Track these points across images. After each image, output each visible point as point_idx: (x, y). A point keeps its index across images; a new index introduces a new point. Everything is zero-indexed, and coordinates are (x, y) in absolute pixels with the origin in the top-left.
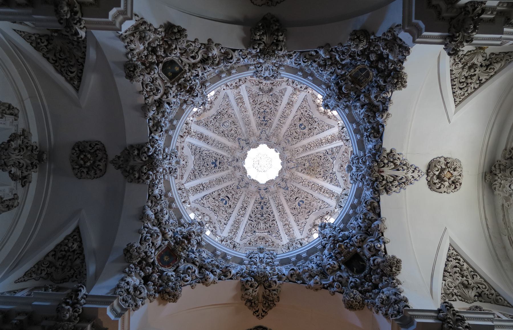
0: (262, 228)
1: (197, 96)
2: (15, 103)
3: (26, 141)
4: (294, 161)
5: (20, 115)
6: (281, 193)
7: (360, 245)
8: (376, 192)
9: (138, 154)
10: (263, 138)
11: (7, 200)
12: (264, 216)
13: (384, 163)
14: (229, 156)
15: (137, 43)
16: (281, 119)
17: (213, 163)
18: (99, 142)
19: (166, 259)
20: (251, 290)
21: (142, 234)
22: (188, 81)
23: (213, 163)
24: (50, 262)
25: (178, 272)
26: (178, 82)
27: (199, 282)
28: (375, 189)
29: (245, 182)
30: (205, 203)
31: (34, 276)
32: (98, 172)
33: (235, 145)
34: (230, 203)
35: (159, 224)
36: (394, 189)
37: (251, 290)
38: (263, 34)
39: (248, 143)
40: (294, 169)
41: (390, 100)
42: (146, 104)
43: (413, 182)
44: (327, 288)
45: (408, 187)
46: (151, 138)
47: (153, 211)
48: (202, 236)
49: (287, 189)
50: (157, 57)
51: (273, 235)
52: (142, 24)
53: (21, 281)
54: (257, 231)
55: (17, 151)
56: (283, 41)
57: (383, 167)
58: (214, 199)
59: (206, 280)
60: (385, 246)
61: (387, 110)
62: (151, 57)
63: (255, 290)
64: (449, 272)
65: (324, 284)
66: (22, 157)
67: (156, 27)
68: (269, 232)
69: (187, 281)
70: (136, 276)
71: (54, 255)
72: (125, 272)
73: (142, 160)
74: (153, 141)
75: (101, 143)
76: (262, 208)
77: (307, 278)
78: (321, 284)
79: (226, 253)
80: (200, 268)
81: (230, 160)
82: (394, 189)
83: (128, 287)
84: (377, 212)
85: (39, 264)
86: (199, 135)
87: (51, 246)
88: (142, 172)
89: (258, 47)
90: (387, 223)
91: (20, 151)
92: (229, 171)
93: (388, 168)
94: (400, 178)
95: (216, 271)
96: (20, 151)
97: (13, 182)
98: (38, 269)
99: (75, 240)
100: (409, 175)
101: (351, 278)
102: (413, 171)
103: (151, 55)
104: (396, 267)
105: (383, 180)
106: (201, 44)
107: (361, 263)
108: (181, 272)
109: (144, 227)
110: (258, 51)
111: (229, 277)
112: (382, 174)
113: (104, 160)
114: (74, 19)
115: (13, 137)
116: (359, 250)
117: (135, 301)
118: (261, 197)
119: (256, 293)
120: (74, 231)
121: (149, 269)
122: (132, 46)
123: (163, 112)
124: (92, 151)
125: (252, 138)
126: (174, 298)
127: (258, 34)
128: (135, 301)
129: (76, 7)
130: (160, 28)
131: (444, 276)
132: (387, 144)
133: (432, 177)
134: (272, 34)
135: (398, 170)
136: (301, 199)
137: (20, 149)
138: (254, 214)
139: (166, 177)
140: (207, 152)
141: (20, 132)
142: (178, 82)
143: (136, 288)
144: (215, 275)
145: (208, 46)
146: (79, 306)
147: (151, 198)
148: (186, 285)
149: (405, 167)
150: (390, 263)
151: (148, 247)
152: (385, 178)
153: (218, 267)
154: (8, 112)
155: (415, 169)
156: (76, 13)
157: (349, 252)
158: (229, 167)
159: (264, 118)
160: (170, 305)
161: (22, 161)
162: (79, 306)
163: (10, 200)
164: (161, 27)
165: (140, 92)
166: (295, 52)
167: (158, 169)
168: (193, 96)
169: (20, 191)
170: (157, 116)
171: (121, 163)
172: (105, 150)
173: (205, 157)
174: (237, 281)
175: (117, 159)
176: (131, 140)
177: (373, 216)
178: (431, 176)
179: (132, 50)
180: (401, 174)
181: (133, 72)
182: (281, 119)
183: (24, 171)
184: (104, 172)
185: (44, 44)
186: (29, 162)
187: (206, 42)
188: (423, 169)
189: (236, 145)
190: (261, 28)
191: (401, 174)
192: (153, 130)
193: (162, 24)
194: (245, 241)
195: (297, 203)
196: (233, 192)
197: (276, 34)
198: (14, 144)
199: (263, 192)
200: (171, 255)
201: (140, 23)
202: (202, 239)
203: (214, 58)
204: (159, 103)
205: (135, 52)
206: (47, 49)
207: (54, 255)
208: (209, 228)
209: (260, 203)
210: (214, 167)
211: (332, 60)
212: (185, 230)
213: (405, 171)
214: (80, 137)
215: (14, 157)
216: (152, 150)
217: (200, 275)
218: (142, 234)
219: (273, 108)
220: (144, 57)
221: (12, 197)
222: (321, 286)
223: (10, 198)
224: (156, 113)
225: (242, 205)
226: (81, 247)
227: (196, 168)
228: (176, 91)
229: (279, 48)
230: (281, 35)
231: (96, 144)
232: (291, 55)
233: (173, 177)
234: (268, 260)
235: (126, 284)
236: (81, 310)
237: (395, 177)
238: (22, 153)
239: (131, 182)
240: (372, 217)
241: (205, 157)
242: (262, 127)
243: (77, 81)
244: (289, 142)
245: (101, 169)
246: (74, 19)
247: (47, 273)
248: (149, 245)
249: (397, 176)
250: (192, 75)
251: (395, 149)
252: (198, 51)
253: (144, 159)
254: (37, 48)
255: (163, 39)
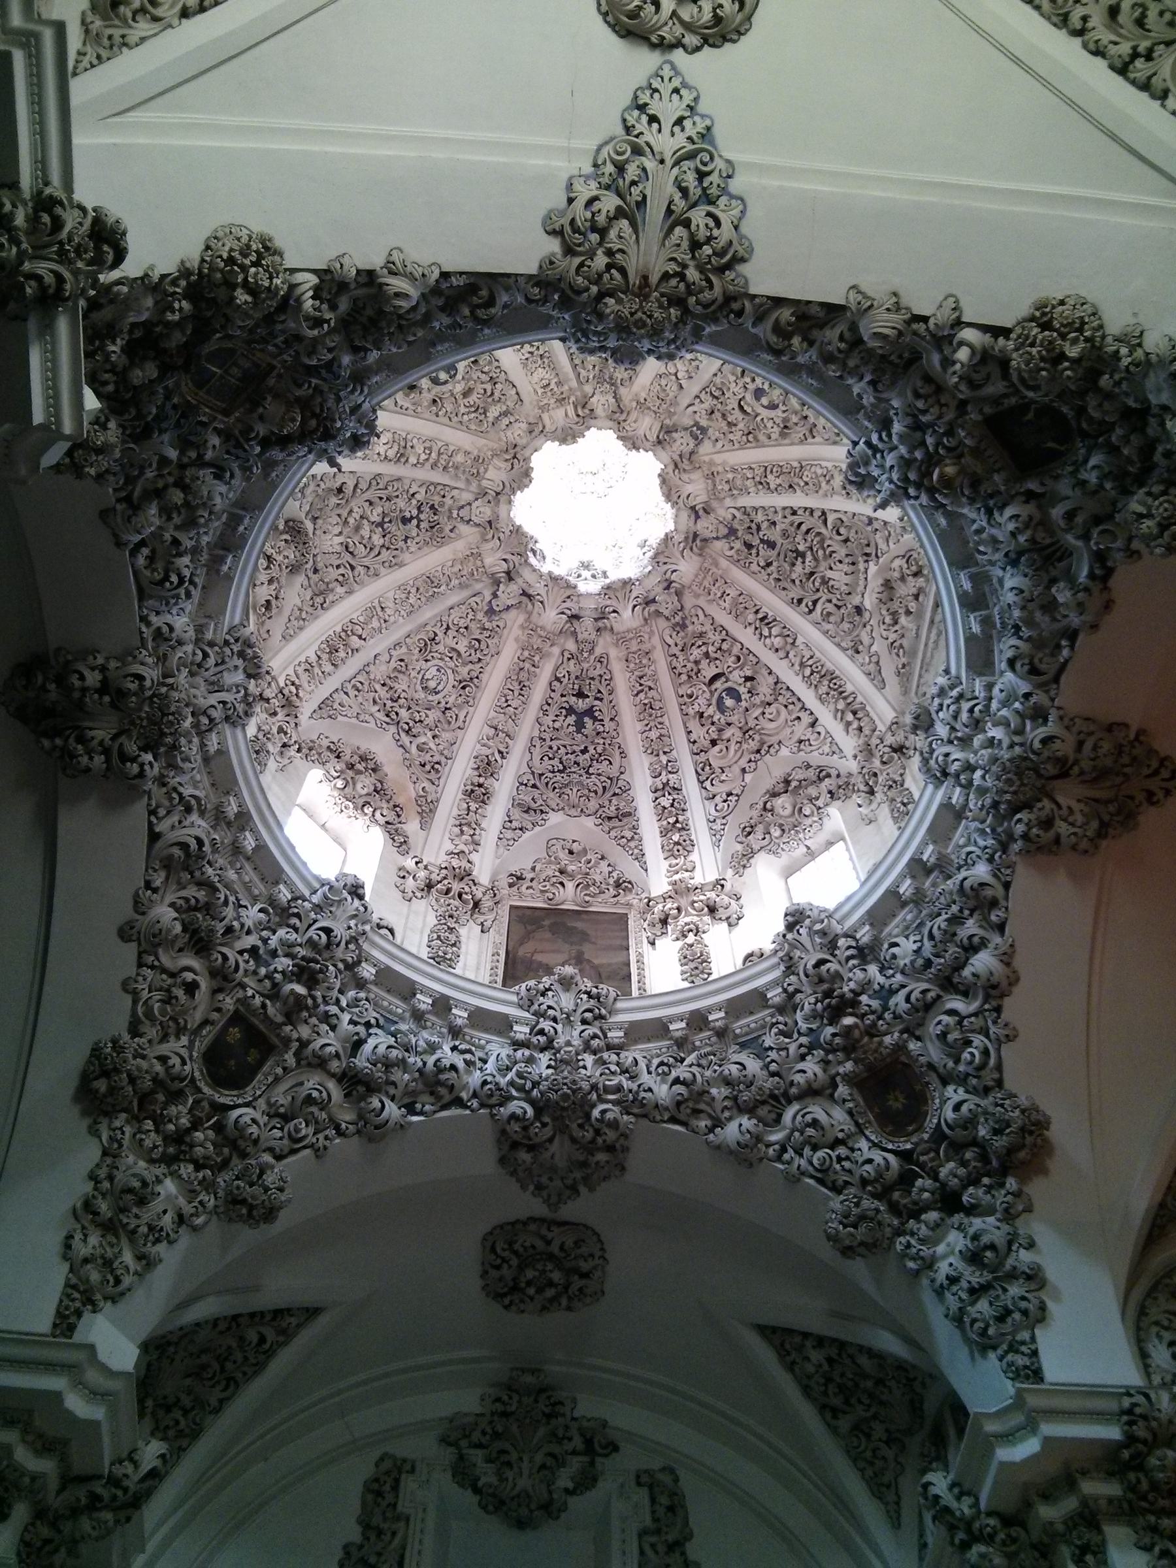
0: (847, 579)
1: (328, 931)
2: (362, 1468)
3: (476, 1436)
4: (588, 389)
5: (403, 1449)
6: (718, 458)
7: (953, 404)
8: (732, 304)
9: (531, 1148)
10: (487, 512)
11: (653, 1512)
12: (801, 548)
13: (609, 267)
14: (556, 650)
15: (156, 1206)
16: (413, 460)
17: (580, 726)
18: (484, 1239)
19: (897, 1102)
20: (1062, 827)
21: (803, 1174)
22: (275, 985)
23: (580, 726)
24: (856, 1428)
25: (950, 1074)
26: (280, 1026)
27: (998, 1010)
28: (721, 307)
29: (661, 598)
30: (725, 788)
31: (888, 1477)
32: (584, 1250)
33: (516, 631)
34: (736, 677)
35: (777, 1100)
36: (725, 233)
37: (1062, 827)
38: (81, 740)
39: (508, 573)
40: (623, 391)
41: (327, 271)
42: (358, 1132)
43: (701, 126)
44: (1109, 572)
45: (728, 147)
46: (475, 1103)
47: (727, 1114)
48: (839, 929)
49: (704, 430)
50: (196, 1125)
51: (882, 546)
52: (96, 1214)
53: (898, 1512)
54: (856, 600)
55: (509, 1474)
56: (103, 669)
57: (623, 271)
58: (714, 743)
59: (994, 987)
60: (970, 325)
61: (371, 273)
62: (199, 1151)
63: (1065, 812)
64: (1135, 55)
65: (1092, 576)
66: (526, 1458)
67: (98, 1153)
68: (867, 555)
69: (986, 1052)
70: (936, 1243)
71: (835, 1412)
72: (917, 1273)
73: (551, 1140)
74: (492, 1097)
75: (491, 1233)
76: (771, 545)
77: (1054, 619)
78: (1087, 590)
79: (912, 860)
80: (949, 983)
81: (571, 646)
82: (725, 233)
83: (964, 1284)
84: (822, 314)
85: (855, 1458)
86: (473, 806)
87: (807, 1413)
88: (593, 1141)
89: (134, 760)
90: (876, 285)
91: (509, 1464)
92: (613, 653)
93: (632, 251)
94: (677, 196)
95: (971, 937)
96: (509, 1464)
97: (600, 1484)
98: (872, 1464)
99: (800, 1349)
100: (667, 143)
101: (1084, 475)
102: (653, 119)
103: (192, 1146)
104: (1063, 336)
105: (682, 276)
106: (140, 965)
107: (1030, 416)
108: (951, 1064)
109: (779, 1159)
110: (149, 757)
111: (999, 891)
112: (654, 279)
113: (544, 1232)
114: (114, 1498)
115: (462, 1473)
116: (974, 416)
117: (1013, 1275)
118: (726, 537)
119: (1076, 807)
120: (770, 1342)
121: (923, 1190)
122: (167, 1220)
123: (388, 1065)
124: (515, 1262)
125: (488, 561)
126: (1035, 1127)
127: (85, 760)
128: (1013, 1275)
129: (78, 1500)
130: (100, 1137)
131: (1145, 86)
132: (523, 250)
133: (688, 27)
134: (80, 705)
135: (642, 203)
136: (749, 397)
137: (500, 1461)
138: (788, 585)
139: (615, 1035)
140: (537, 753)
141: (449, 1454)
142: (280, 1026)
143: (974, 1258)
144: (984, 943)
145: (146, 942)
146: (977, 1525)
147: (682, 1117)
148: (999, 1057)
149: (632, 172)
150: (1042, 359)
151: (846, 1164)
152: (672, 267)
153: (957, 920)
154: (389, 1498)
155: (642, 108)
156: (95, 1498)
157: (976, 452)
158: (598, 651)
159: (405, 521)
160: (1057, 1133)
161: (539, 1458)
162: (977, 1525)
163: (653, 1500)
164: (94, 1131)
165: (319, 1153)
166: (144, 619)
167: (585, 1086)
168: (328, 946)
169: (629, 1460)
170: (401, 1087)
171: (558, 1183)
172: (513, 1224)
173: (556, 762)
174: (1020, 869)
175: (545, 1193)
176: (481, 1160)
177: (837, 332)
178: (679, 30)
179: (181, 1219)
180: (661, 189)
181: (251, 1208)
182: (413, 460)
183: (569, 1446)
184: (584, 1232)
185: (181, 1419)
186: (542, 1431)
187: (131, 950)
188: (642, 63)
189: (515, 619)
190: (58, 741)
191: (661, 189)
192: (447, 1098)
193: (86, 1122)
194: (888, 672)
195: (765, 413)
196: (696, 653)
197: (76, 695)
198: (487, 1476)
199: (705, 526)
200: (889, 1087)
201: (93, 1221)
202: (846, 936)
203: (186, 909)
204: (357, 1084)
205: (188, 1209)
206: (193, 1408)
207: (835, 1412)
208: (820, 803)
209: (749, 546)
210: (595, 719)
211: (166, 487)
212: (808, 1001)
213: (650, 164)
214: (474, 1283)
215: (523, 1483)
216: (517, 1106)
217: (975, 997)
218: (803, 1174)
219: (367, 496)
220: (201, 1175)
221: (642, 1496)
222: (1096, 588)
223: (647, 1501)
224: (392, 1091)
225: (751, 630)
226: (821, 1342)
227: (593, 805)
228: (314, 1020)
229: (133, 686)
230: (82, 678)
231: (493, 1249)
232: (158, 633)
233: (620, 1005)
234: (964, 716)
235: (954, 1288)
236: (992, 1522)
237: (675, 220)
238: (514, 1456)
239: (623, 1169)
240: (841, 338)
241: (556, 762)
242: (443, 519)
243: (283, 1321)
244: (505, 414)
245: (576, 1243)
246: (114, 1498)
247: (887, 1443)
248: (840, 1159)
249: (669, 211)
250: (255, 973)
251: (548, 218)
252: (164, 970)
253: (548, 1132)
254: (195, 1433)
255: (137, 1119)
